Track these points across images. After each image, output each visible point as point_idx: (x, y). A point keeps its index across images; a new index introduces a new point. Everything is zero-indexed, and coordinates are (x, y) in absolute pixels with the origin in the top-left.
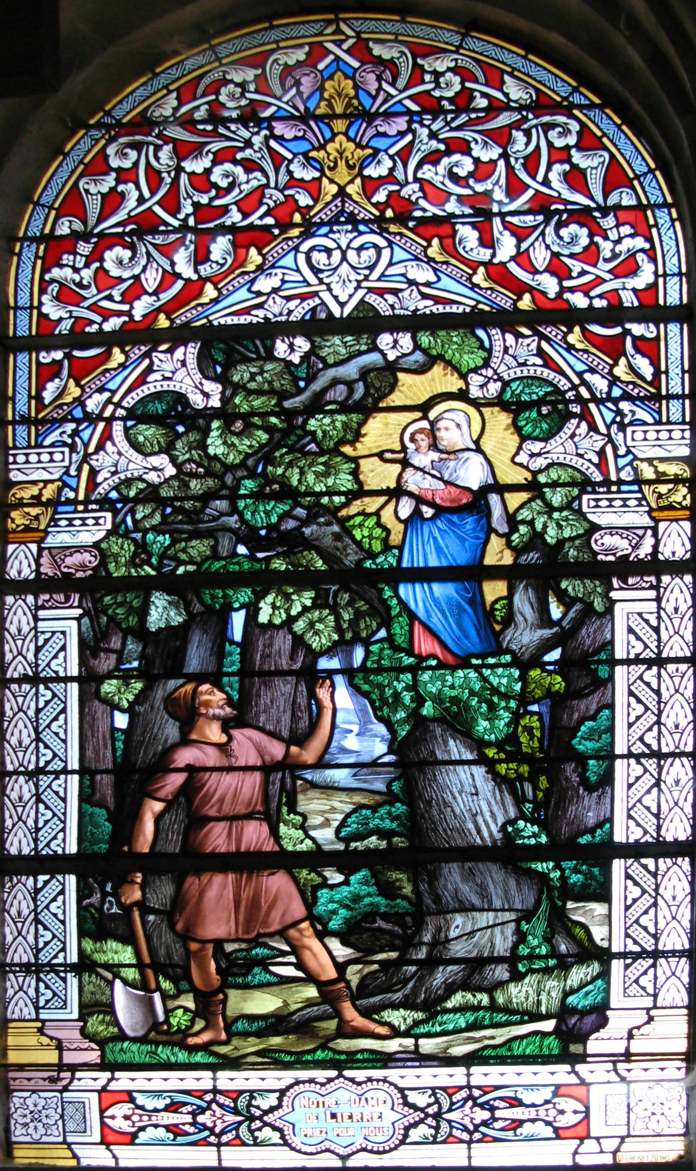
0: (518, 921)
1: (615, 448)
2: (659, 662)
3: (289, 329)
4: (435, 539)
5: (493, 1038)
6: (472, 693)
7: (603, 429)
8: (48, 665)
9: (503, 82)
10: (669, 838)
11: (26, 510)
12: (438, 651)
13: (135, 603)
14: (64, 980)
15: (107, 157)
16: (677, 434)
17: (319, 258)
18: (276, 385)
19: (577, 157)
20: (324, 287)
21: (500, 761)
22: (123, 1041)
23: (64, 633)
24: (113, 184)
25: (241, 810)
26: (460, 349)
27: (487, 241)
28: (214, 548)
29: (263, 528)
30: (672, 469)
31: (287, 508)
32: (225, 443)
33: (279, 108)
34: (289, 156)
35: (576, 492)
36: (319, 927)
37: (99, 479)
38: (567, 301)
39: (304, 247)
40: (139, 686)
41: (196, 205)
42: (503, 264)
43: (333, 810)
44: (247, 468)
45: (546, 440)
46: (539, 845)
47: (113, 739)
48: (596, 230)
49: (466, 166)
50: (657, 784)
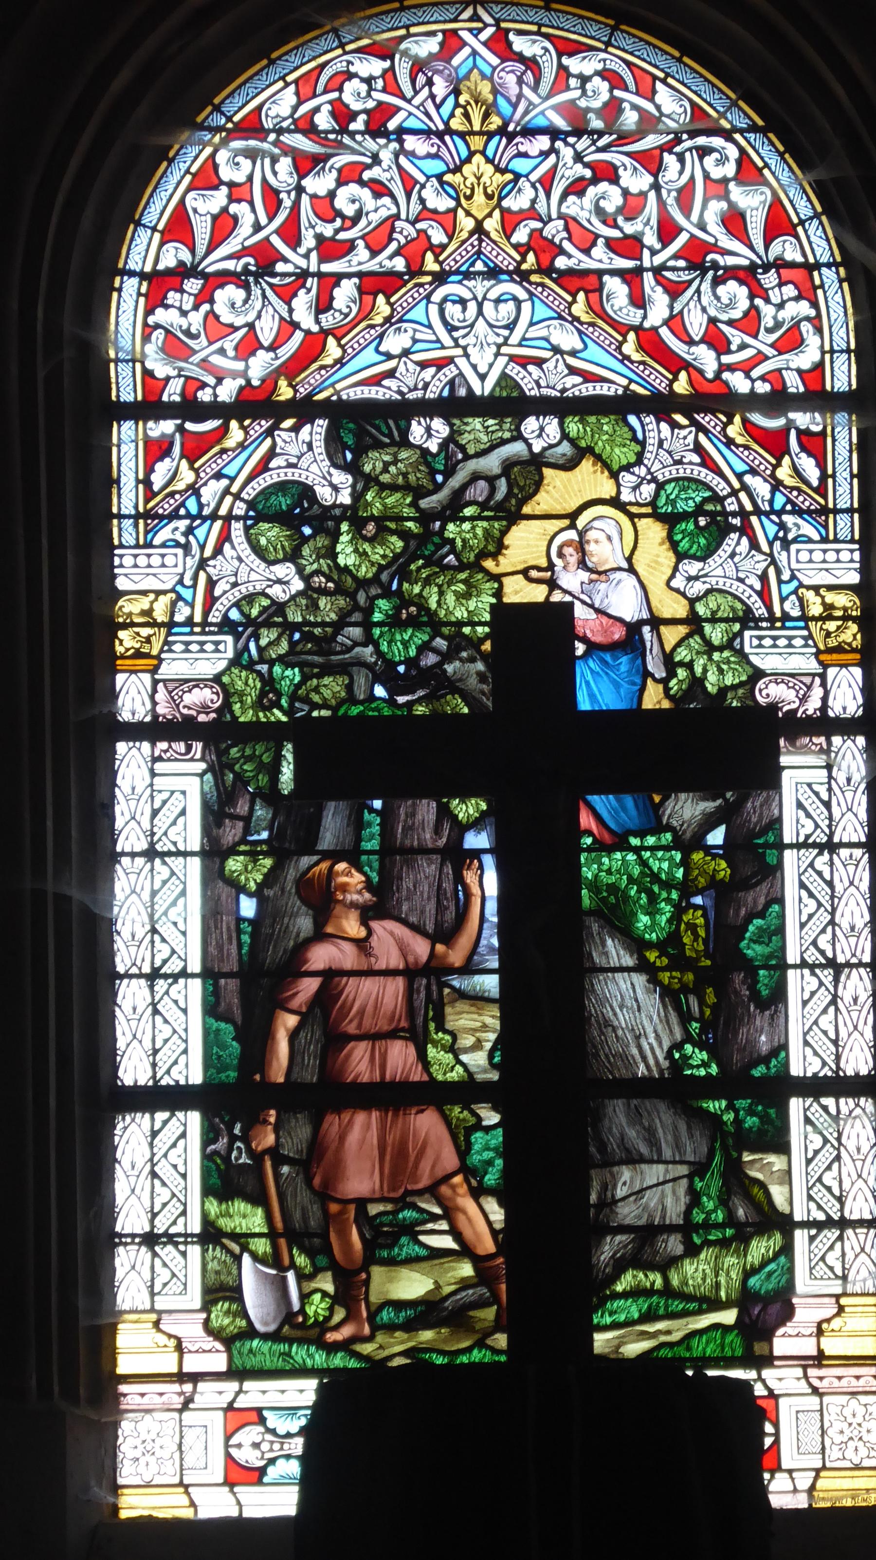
0: (690, 1177)
1: (778, 572)
2: (831, 847)
3: (427, 408)
4: (588, 683)
5: (668, 1332)
6: (631, 880)
7: (765, 547)
8: (165, 834)
9: (654, 92)
10: (850, 1072)
11: (136, 629)
12: (594, 827)
13: (266, 758)
14: (184, 1254)
15: (216, 167)
16: (845, 556)
17: (453, 311)
18: (412, 478)
19: (736, 192)
20: (460, 351)
21: (663, 969)
22: (252, 1339)
23: (184, 793)
24: (224, 202)
25: (384, 1026)
26: (611, 441)
27: (639, 300)
28: (349, 688)
29: (400, 663)
30: (842, 600)
31: (426, 638)
32: (356, 551)
33: (410, 114)
34: (422, 179)
35: (737, 627)
36: (474, 1183)
37: (217, 592)
38: (726, 383)
39: (437, 297)
40: (268, 862)
41: (319, 238)
42: (655, 330)
43: (485, 1027)
44: (380, 584)
45: (703, 559)
46: (709, 1075)
47: (239, 932)
48: (757, 291)
49: (613, 200)
50: (834, 1002)
